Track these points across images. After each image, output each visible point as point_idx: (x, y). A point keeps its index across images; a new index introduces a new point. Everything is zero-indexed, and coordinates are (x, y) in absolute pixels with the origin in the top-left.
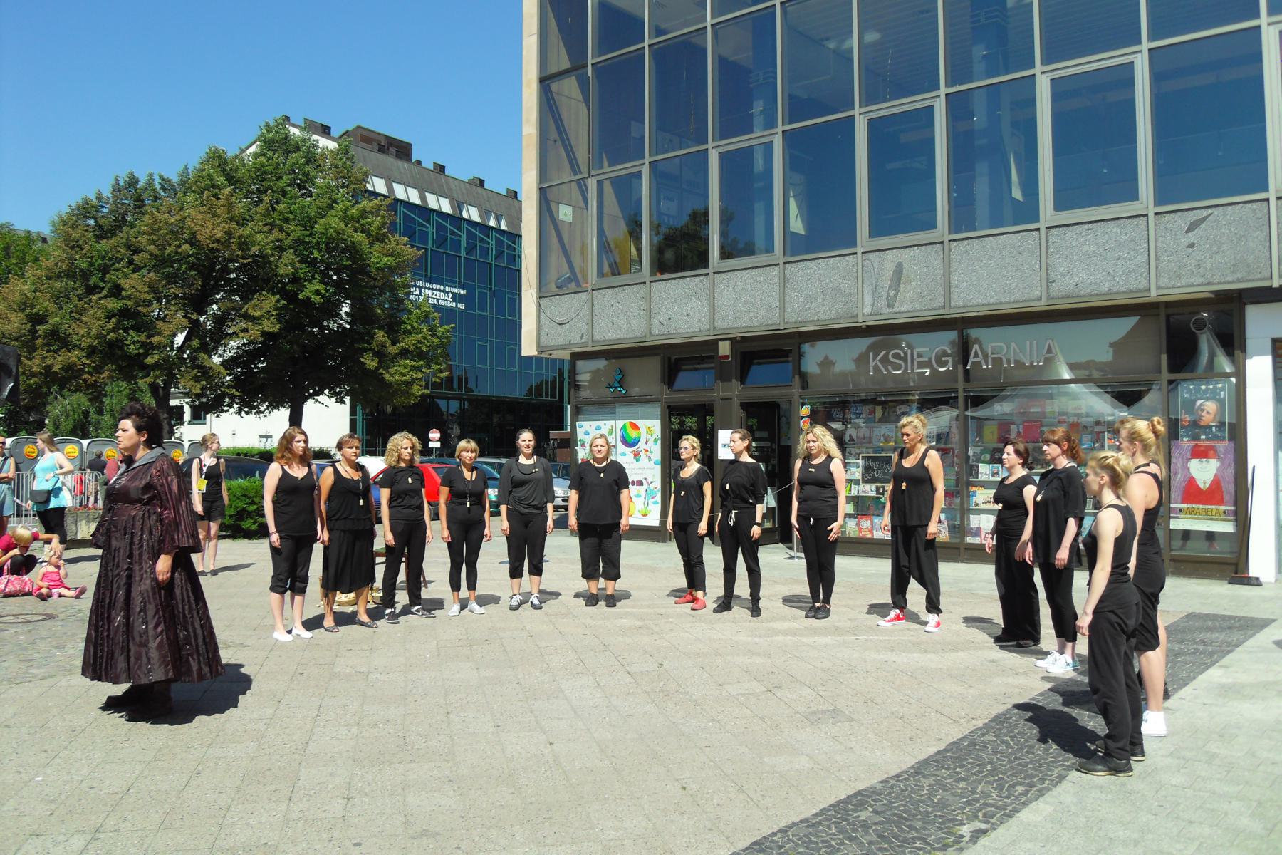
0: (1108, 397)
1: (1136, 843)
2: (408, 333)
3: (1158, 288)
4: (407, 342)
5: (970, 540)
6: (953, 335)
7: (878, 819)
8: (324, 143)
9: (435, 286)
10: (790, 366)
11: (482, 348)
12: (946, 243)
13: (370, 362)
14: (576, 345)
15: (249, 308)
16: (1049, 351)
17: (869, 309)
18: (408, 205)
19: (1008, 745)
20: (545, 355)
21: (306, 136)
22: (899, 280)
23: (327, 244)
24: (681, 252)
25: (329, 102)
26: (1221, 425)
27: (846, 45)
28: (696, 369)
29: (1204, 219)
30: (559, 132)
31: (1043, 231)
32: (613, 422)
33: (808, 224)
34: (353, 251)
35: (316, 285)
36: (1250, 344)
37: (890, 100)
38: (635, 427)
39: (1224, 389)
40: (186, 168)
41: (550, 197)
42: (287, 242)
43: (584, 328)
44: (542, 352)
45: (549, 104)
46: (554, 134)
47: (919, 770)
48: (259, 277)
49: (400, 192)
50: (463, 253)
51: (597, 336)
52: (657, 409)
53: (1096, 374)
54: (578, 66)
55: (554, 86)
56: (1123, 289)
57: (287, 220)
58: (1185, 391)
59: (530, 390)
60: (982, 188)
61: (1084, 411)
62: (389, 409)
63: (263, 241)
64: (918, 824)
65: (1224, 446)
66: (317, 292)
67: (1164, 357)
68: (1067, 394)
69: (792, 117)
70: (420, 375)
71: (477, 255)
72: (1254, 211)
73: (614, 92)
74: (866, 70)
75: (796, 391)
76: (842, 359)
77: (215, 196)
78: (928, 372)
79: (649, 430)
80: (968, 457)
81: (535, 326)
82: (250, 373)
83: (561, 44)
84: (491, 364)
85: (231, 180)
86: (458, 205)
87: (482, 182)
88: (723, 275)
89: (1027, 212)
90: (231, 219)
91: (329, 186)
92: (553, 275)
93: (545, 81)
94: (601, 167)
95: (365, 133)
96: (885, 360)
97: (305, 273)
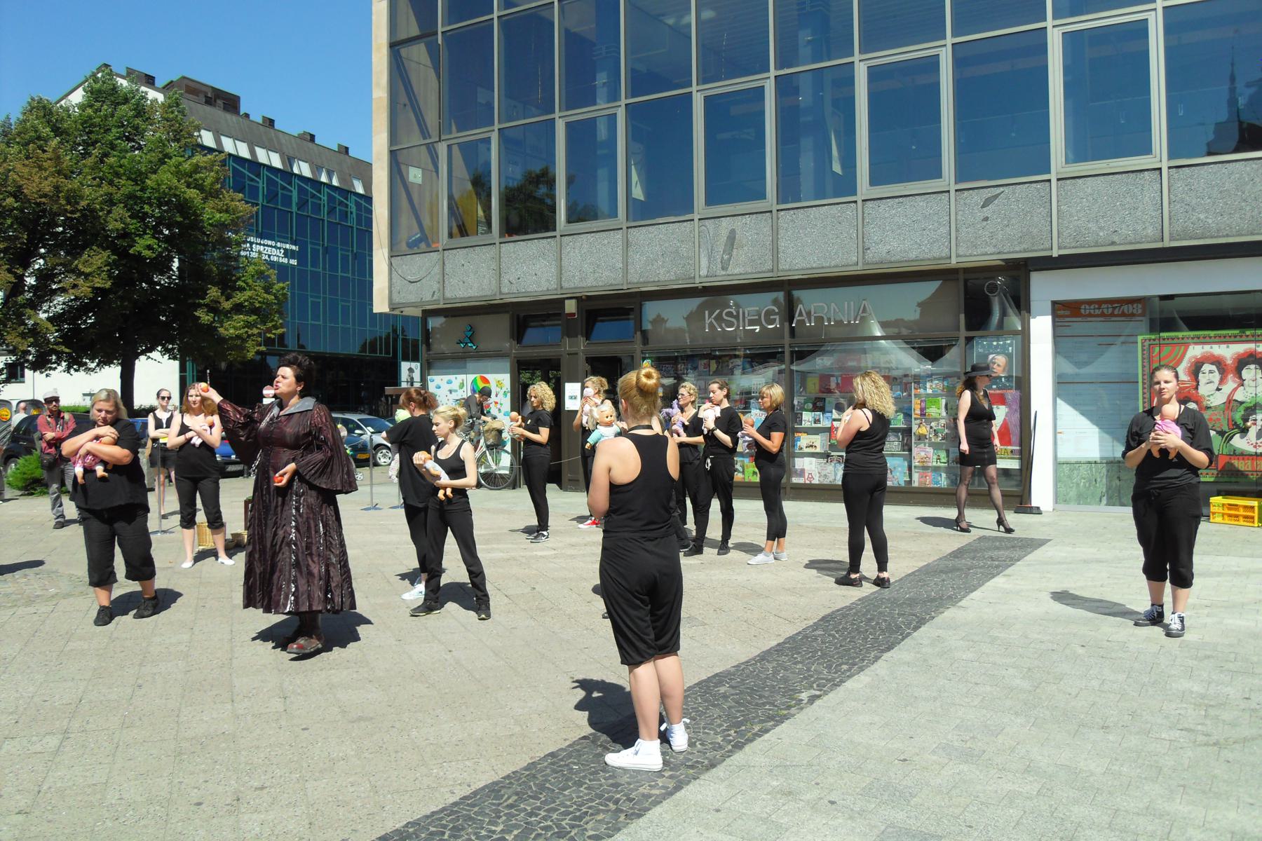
0: (914, 352)
1: (935, 699)
2: (242, 289)
3: (958, 256)
4: (240, 297)
5: (795, 480)
6: (780, 295)
7: (733, 691)
8: (152, 94)
9: (266, 242)
10: (632, 323)
11: (345, 309)
12: (774, 212)
13: (205, 317)
14: (429, 303)
15: (78, 264)
16: (864, 310)
17: (705, 271)
18: (237, 159)
19: (834, 637)
20: (397, 312)
21: (134, 87)
22: (732, 245)
23: (158, 199)
24: (528, 214)
25: (160, 57)
26: (1009, 378)
27: (684, 21)
28: (543, 326)
29: (996, 196)
30: (410, 99)
31: (860, 203)
32: (463, 376)
33: (647, 193)
34: (184, 207)
35: (148, 240)
36: (1034, 306)
37: (726, 79)
38: (485, 380)
39: (1011, 344)
40: (8, 118)
41: (401, 158)
42: (117, 197)
43: (436, 286)
44: (393, 309)
45: (398, 67)
46: (403, 98)
47: (764, 657)
48: (86, 232)
49: (228, 145)
50: (294, 209)
51: (448, 295)
52: (506, 364)
53: (905, 332)
54: (427, 34)
55: (404, 52)
56: (928, 256)
57: (118, 175)
58: (980, 347)
59: (363, 349)
60: (807, 163)
61: (893, 365)
62: (223, 365)
63: (91, 194)
64: (767, 694)
65: (1012, 394)
66: (149, 247)
67: (962, 317)
68: (879, 349)
69: (635, 91)
70: (255, 331)
71: (308, 211)
72: (1038, 190)
73: (463, 63)
74: (703, 48)
75: (638, 346)
76: (672, 319)
77: (40, 147)
78: (758, 329)
79: (499, 383)
80: (793, 406)
81: (387, 284)
82: (76, 331)
83: (411, 11)
84: (325, 322)
85: (57, 131)
86: (288, 160)
87: (312, 137)
88: (570, 238)
89: (846, 186)
90: (59, 172)
91: (161, 141)
92: (403, 235)
93: (395, 46)
94: (450, 133)
95: (191, 84)
96: (719, 318)
97: (136, 229)
